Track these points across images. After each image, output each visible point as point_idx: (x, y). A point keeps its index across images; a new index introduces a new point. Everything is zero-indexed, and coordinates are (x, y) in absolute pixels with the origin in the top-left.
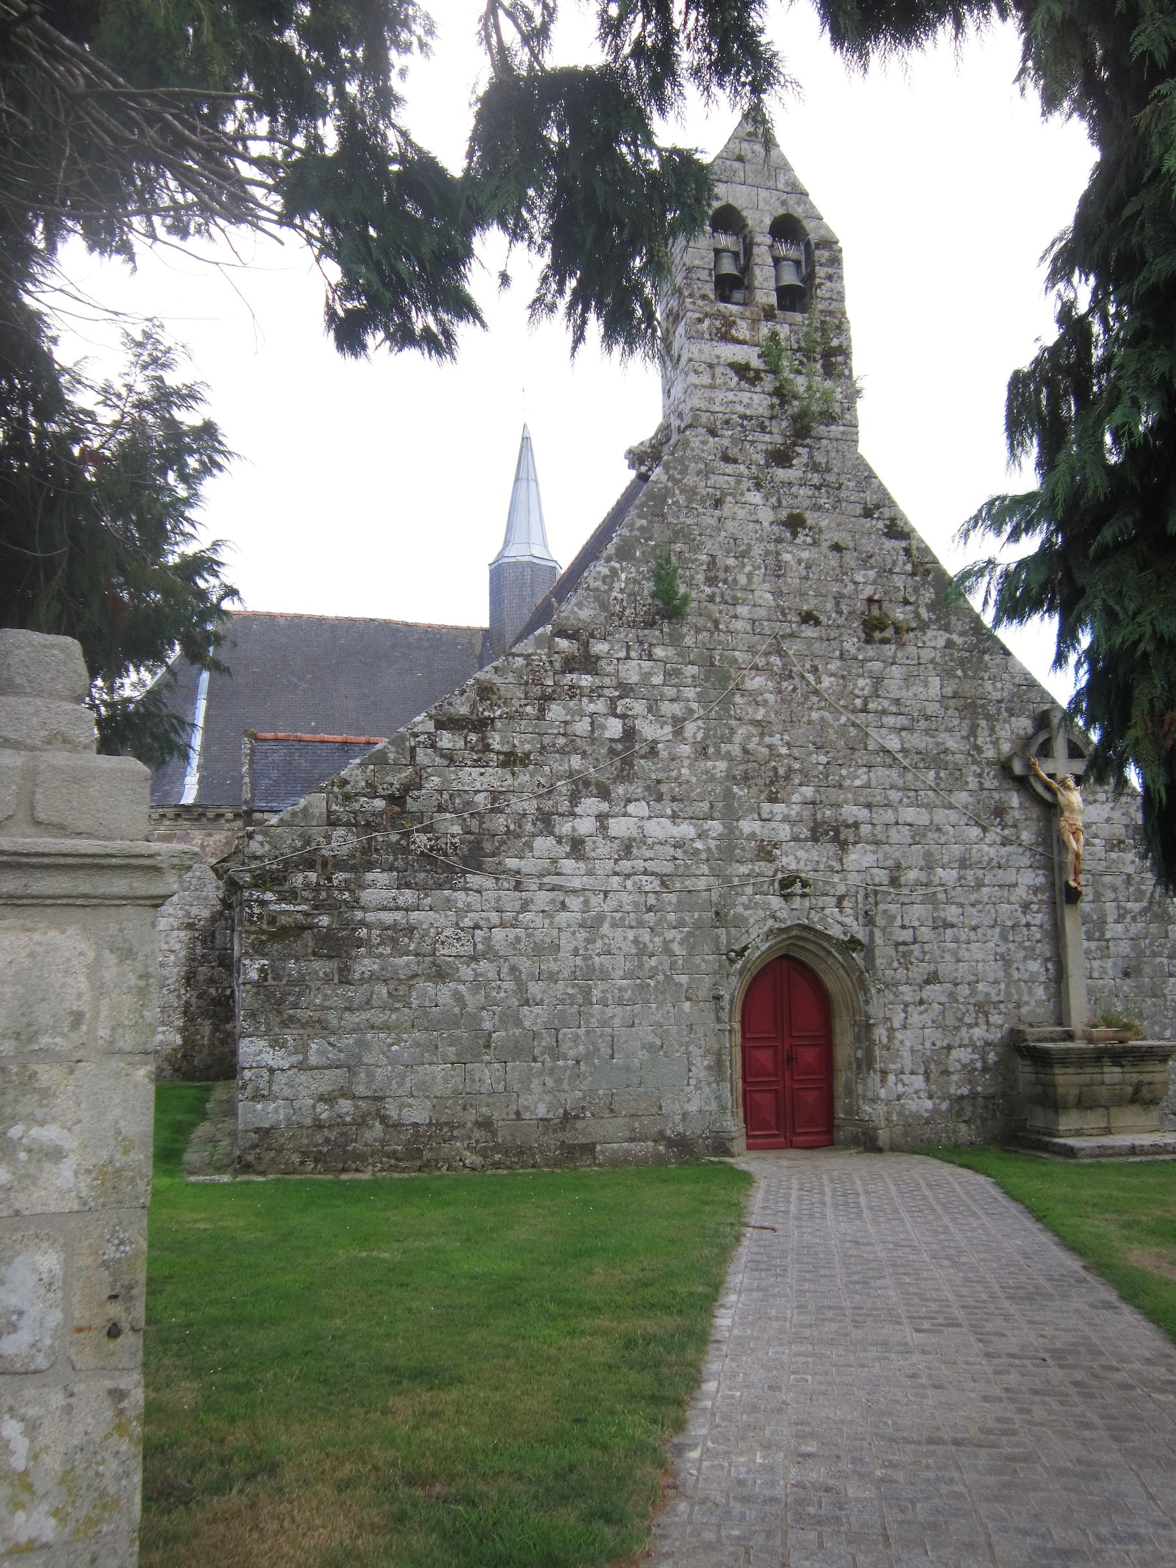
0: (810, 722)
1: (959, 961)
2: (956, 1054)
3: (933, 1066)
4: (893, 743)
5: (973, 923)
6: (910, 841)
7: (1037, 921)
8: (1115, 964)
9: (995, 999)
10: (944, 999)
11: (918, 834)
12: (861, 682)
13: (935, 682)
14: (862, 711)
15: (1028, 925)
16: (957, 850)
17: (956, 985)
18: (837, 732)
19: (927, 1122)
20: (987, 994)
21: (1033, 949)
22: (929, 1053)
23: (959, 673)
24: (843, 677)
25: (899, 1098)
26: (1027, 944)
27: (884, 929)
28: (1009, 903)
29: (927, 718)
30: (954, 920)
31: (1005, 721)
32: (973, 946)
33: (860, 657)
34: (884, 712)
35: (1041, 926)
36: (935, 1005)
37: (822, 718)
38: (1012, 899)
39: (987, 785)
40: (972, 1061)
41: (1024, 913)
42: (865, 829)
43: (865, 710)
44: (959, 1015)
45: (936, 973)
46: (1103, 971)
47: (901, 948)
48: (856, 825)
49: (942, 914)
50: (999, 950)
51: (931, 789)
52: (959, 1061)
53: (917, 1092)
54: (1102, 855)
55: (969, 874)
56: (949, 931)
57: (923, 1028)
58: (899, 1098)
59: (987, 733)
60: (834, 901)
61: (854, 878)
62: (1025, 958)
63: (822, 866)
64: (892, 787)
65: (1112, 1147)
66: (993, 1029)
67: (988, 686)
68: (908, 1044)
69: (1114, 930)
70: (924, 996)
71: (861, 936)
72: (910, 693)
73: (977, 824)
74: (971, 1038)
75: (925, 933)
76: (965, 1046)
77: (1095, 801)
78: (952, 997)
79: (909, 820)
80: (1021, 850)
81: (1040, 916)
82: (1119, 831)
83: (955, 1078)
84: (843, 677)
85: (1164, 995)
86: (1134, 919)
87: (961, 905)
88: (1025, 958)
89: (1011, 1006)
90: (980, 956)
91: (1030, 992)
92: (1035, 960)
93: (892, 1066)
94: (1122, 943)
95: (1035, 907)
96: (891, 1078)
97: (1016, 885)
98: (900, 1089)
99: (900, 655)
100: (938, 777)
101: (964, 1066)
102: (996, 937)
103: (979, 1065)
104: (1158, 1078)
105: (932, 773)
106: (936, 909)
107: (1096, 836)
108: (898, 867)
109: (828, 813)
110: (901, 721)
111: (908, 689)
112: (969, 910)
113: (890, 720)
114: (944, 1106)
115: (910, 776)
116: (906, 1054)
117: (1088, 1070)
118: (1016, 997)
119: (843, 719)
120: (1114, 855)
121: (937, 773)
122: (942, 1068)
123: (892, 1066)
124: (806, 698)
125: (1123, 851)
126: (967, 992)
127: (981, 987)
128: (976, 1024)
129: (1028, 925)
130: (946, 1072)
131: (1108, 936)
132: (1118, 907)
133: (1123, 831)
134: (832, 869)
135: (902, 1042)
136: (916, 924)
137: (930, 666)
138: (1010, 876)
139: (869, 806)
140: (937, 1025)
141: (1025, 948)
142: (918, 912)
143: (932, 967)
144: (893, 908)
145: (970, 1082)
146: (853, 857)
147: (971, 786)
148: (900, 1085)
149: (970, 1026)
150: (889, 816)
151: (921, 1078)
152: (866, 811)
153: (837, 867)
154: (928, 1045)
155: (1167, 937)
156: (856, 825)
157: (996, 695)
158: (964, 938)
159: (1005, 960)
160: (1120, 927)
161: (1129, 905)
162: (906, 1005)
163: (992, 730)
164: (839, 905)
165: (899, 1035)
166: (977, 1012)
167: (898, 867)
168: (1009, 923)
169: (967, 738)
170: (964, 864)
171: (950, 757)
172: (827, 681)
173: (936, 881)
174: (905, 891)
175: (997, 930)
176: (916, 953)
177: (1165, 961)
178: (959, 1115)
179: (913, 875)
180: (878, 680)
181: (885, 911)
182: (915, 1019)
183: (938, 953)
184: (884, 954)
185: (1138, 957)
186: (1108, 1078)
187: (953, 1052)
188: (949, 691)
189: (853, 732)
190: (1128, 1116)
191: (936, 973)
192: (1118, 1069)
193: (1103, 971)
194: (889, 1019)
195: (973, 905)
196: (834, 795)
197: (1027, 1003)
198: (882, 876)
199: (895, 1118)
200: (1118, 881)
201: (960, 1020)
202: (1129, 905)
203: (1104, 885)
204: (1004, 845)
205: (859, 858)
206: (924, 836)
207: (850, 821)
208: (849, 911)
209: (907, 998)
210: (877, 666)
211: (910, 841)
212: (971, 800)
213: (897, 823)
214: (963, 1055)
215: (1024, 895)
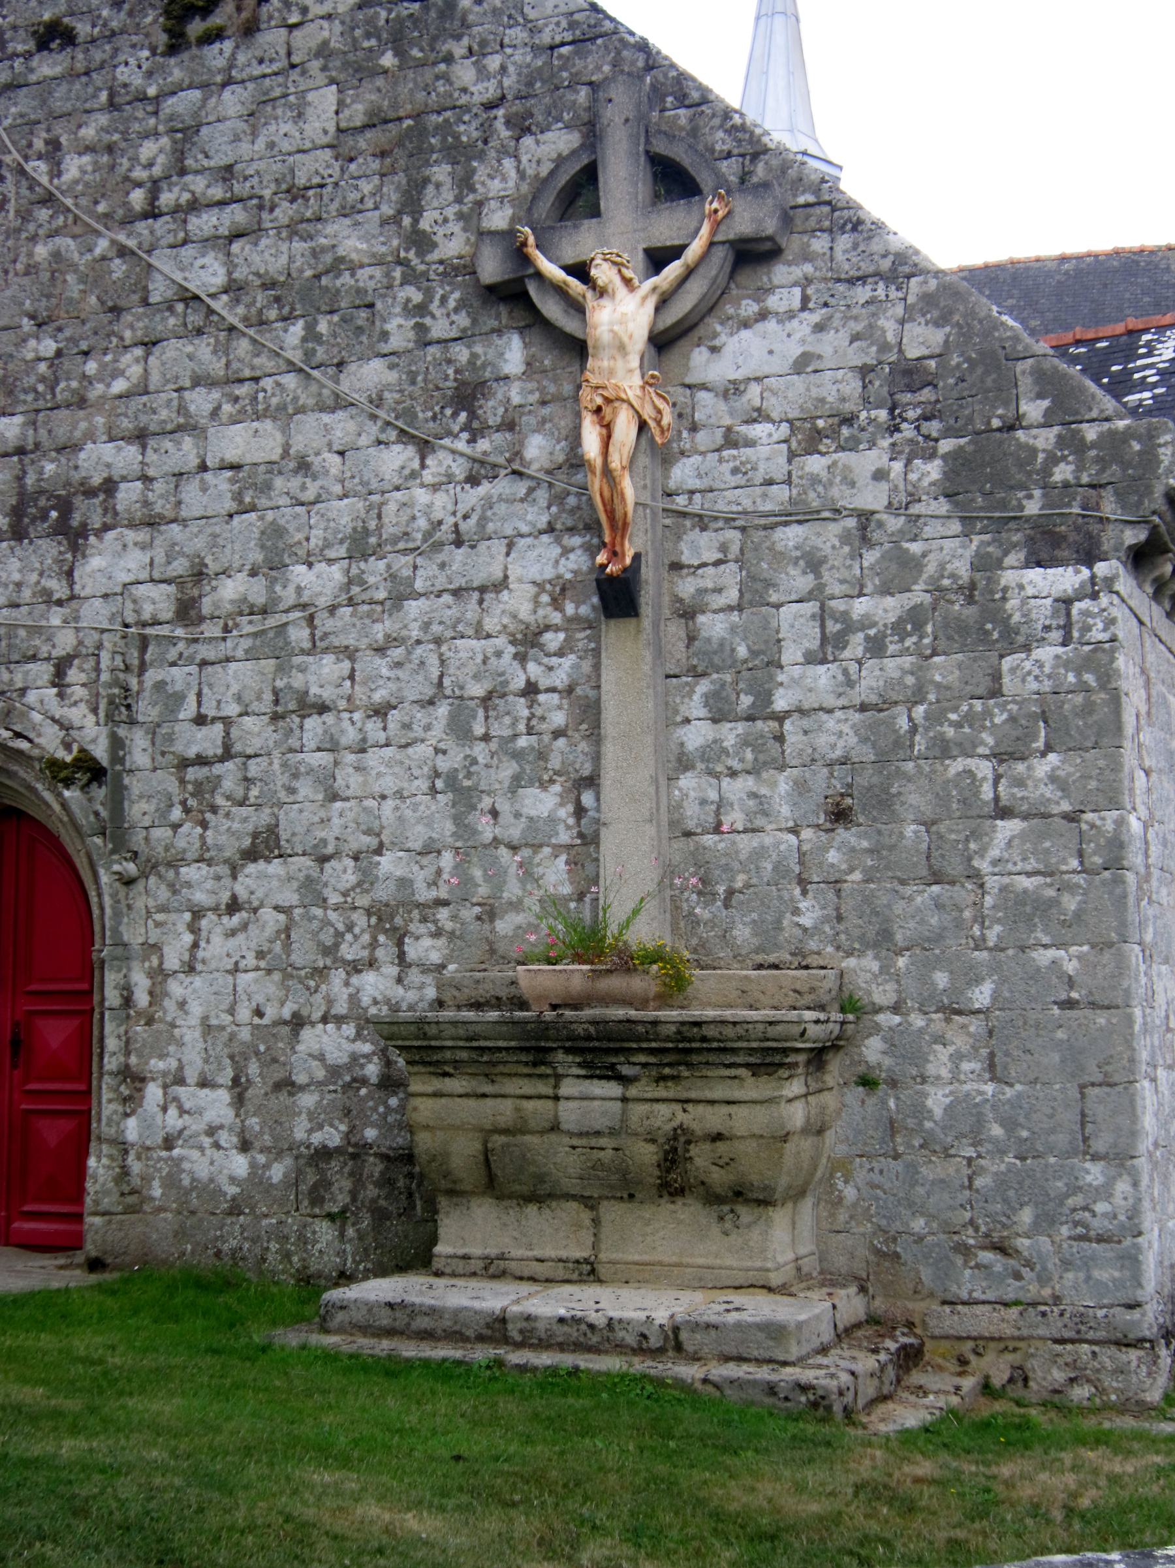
0: (31, 270)
1: (334, 797)
2: (312, 1038)
3: (253, 1068)
4: (207, 274)
5: (378, 697)
6: (229, 505)
7: (560, 678)
8: (801, 787)
9: (425, 895)
10: (289, 897)
11: (249, 483)
12: (148, 149)
13: (325, 100)
14: (145, 216)
15: (531, 690)
16: (344, 513)
17: (323, 859)
18: (83, 279)
19: (235, 1209)
20: (404, 883)
21: (542, 755)
22: (245, 1034)
23: (388, 60)
24: (110, 149)
25: (169, 1143)
26: (523, 742)
27: (153, 731)
28: (481, 634)
29: (295, 193)
30: (327, 694)
31: (503, 152)
32: (373, 758)
33: (152, 91)
34: (194, 206)
35: (570, 690)
36: (267, 914)
37: (56, 255)
38: (490, 624)
39: (439, 328)
40: (354, 1057)
41: (521, 658)
42: (128, 495)
43: (152, 213)
44: (327, 938)
45: (272, 830)
46: (761, 806)
47: (192, 773)
48: (109, 487)
49: (298, 680)
50: (443, 764)
51: (292, 368)
52: (321, 1058)
53: (211, 1131)
54: (779, 466)
55: (375, 569)
56: (313, 723)
57: (236, 970)
58: (169, 1143)
59: (448, 195)
60: (42, 671)
61: (95, 613)
62: (517, 782)
63: (27, 594)
64: (197, 382)
65: (432, 1312)
66: (414, 976)
67: (465, 73)
68: (196, 1009)
69: (801, 682)
70: (243, 895)
71: (100, 752)
72: (260, 144)
73: (404, 436)
74: (354, 999)
75: (255, 732)
76: (340, 1020)
77: (763, 316)
78: (312, 892)
79: (231, 456)
80: (521, 488)
81: (568, 661)
82: (838, 387)
83: (307, 1100)
84: (110, 149)
85: (975, 876)
86: (876, 647)
87: (349, 653)
88: (517, 782)
89: (469, 913)
90: (388, 784)
91: (528, 874)
92: (544, 786)
93: (157, 1065)
94: (830, 722)
95: (553, 640)
96: (153, 1093)
97: (502, 585)
98: (173, 1120)
99: (241, 58)
100: (311, 334)
101: (334, 1071)
102: (438, 731)
103: (372, 1070)
104: (743, 1120)
105: (297, 329)
106: (282, 669)
107: (759, 415)
108: (199, 574)
109: (50, 468)
110: (237, 215)
111: (254, 134)
112: (371, 664)
113: (204, 223)
114: (277, 1172)
115: (243, 346)
116: (190, 1033)
117: (512, 1086)
118: (483, 891)
119: (102, 246)
120: (815, 464)
121: (310, 328)
122: (278, 1074)
123: (157, 1065)
124: (25, 216)
125: (851, 446)
126: (351, 878)
127: (387, 863)
128: (372, 963)
129: (531, 690)
130: (286, 1085)
131: (781, 702)
132: (822, 617)
133: (853, 386)
134: (48, 599)
135: (182, 1004)
136: (232, 709)
137: (316, 65)
138: (487, 562)
139: (141, 437)
140: (275, 963)
141: (517, 755)
142: (241, 679)
143: (264, 818)
144: (178, 676)
145: (347, 1112)
146: (96, 562)
147: (397, 342)
148: (173, 1112)
149: (355, 968)
150: (186, 452)
151: (224, 1096)
152: (132, 451)
153: (59, 589)
154: (244, 1013)
155: (995, 692)
156: (109, 487)
157: (486, 91)
158: (350, 735)
159: (461, 791)
160: (823, 676)
161: (860, 607)
162: (198, 914)
163: (465, 183)
164: (59, 680)
165: (176, 988)
166: (375, 930)
167: (199, 574)
168: (477, 690)
169: (396, 220)
170: (361, 545)
171: (346, 278)
172: (74, 166)
173: (288, 596)
174: (211, 630)
175: (443, 710)
176: (228, 785)
177: (984, 769)
178: (316, 1198)
179: (230, 590)
180: (185, 134)
181: (160, 686)
182: (216, 948)
183: (282, 779)
184: (148, 790)
185: (881, 761)
186: (569, 1114)
187: (306, 1033)
188: (357, 113)
189: (119, 268)
190: (666, 1231)
191: (272, 830)
192: (613, 1089)
193: (761, 806)
194: (156, 948)
195: (380, 650)
196: (63, 424)
197: (516, 906)
198: (158, 600)
199: (157, 1192)
200: (827, 538)
201: (329, 951)
202: (860, 607)
203: (779, 557)
204: (473, 480)
205: (112, 562)
206: (268, 487)
207: (96, 480)
208: (79, 692)
209: (200, 897)
210: (183, 103)
211: (229, 505)
212: (392, 377)
213: (203, 467)
214: (331, 1043)
215: (524, 610)
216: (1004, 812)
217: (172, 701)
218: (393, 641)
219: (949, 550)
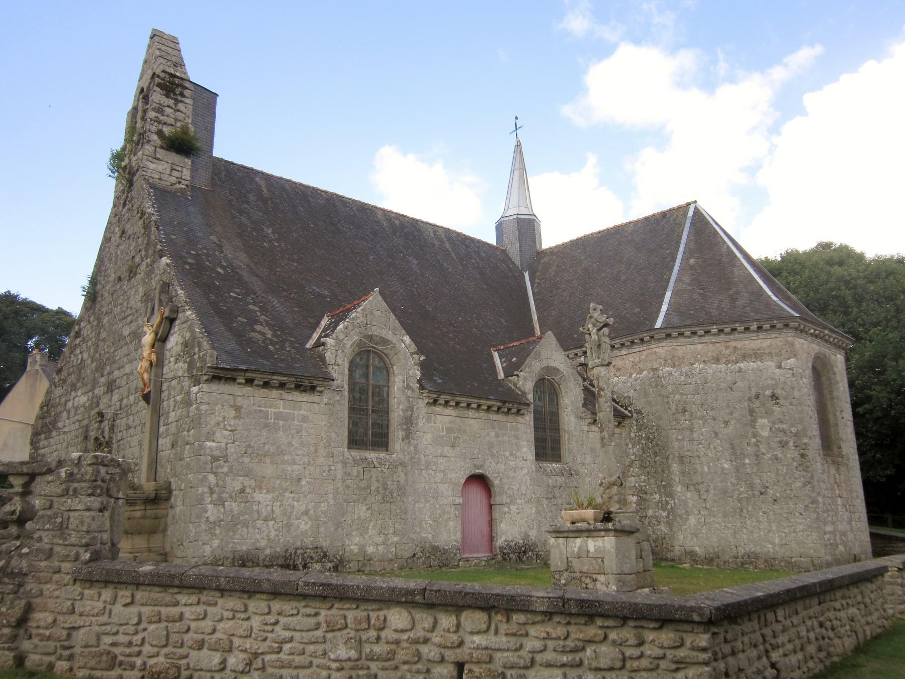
177: (186, 433)
219: (186, 383)
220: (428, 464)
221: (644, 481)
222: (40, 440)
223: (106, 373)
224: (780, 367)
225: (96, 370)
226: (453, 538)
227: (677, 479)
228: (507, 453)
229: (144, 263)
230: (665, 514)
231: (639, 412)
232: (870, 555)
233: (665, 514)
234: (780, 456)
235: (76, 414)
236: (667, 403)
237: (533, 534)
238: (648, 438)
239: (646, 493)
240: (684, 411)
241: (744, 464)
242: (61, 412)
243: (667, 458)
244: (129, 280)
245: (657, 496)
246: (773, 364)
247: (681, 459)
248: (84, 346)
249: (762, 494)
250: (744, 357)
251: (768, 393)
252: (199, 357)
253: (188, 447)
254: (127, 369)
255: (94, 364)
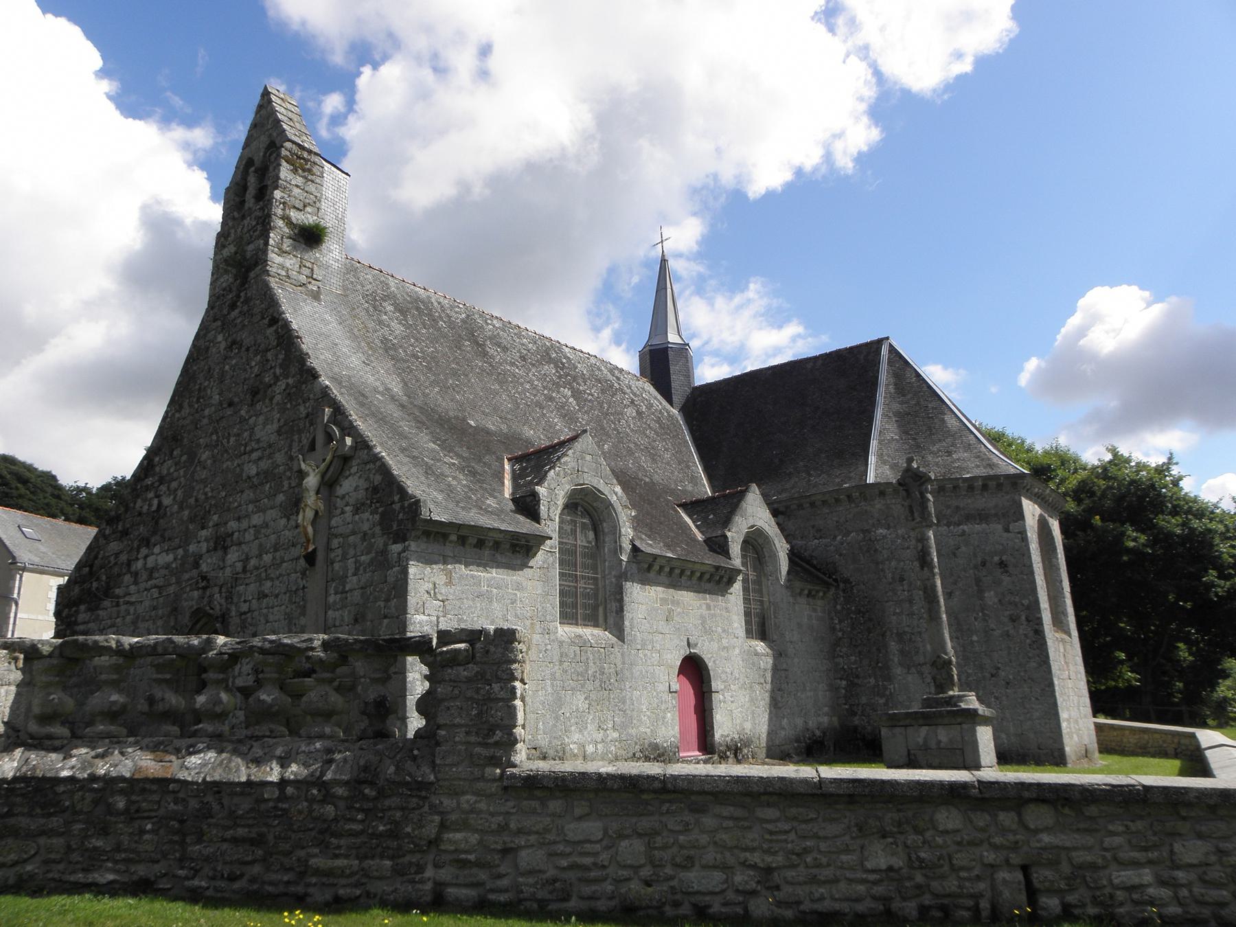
34: (252, 451)
82: (361, 494)
113: (255, 455)
172: (232, 439)
177: (382, 604)
216: (386, 617)
217: (240, 596)
218: (281, 575)
219: (380, 542)
220: (644, 645)
221: (855, 662)
222: (77, 612)
223: (211, 524)
224: (1007, 530)
225: (192, 520)
226: (672, 732)
227: (896, 660)
228: (719, 630)
229: (282, 384)
230: (882, 701)
231: (847, 581)
232: (762, 754)
233: (882, 701)
234: (1012, 632)
235: (150, 578)
236: (883, 570)
237: (748, 726)
238: (859, 612)
239: (858, 677)
240: (902, 580)
241: (972, 642)
242: (119, 575)
243: (883, 635)
244: (252, 405)
245: (872, 681)
246: (1000, 527)
247: (900, 636)
248: (163, 488)
249: (993, 676)
250: (968, 518)
251: (996, 559)
252: (402, 507)
253: (386, 621)
254: (257, 519)
255: (186, 513)
